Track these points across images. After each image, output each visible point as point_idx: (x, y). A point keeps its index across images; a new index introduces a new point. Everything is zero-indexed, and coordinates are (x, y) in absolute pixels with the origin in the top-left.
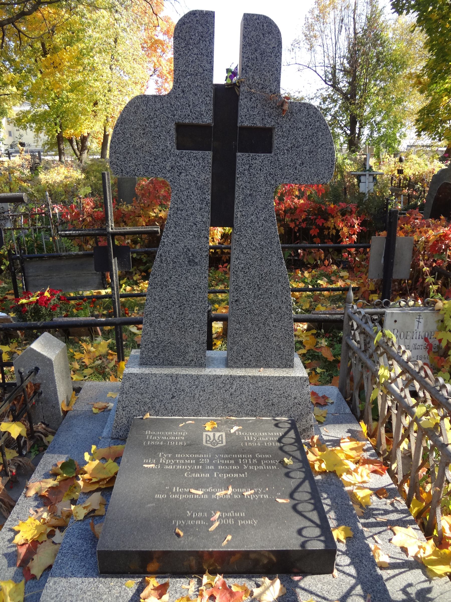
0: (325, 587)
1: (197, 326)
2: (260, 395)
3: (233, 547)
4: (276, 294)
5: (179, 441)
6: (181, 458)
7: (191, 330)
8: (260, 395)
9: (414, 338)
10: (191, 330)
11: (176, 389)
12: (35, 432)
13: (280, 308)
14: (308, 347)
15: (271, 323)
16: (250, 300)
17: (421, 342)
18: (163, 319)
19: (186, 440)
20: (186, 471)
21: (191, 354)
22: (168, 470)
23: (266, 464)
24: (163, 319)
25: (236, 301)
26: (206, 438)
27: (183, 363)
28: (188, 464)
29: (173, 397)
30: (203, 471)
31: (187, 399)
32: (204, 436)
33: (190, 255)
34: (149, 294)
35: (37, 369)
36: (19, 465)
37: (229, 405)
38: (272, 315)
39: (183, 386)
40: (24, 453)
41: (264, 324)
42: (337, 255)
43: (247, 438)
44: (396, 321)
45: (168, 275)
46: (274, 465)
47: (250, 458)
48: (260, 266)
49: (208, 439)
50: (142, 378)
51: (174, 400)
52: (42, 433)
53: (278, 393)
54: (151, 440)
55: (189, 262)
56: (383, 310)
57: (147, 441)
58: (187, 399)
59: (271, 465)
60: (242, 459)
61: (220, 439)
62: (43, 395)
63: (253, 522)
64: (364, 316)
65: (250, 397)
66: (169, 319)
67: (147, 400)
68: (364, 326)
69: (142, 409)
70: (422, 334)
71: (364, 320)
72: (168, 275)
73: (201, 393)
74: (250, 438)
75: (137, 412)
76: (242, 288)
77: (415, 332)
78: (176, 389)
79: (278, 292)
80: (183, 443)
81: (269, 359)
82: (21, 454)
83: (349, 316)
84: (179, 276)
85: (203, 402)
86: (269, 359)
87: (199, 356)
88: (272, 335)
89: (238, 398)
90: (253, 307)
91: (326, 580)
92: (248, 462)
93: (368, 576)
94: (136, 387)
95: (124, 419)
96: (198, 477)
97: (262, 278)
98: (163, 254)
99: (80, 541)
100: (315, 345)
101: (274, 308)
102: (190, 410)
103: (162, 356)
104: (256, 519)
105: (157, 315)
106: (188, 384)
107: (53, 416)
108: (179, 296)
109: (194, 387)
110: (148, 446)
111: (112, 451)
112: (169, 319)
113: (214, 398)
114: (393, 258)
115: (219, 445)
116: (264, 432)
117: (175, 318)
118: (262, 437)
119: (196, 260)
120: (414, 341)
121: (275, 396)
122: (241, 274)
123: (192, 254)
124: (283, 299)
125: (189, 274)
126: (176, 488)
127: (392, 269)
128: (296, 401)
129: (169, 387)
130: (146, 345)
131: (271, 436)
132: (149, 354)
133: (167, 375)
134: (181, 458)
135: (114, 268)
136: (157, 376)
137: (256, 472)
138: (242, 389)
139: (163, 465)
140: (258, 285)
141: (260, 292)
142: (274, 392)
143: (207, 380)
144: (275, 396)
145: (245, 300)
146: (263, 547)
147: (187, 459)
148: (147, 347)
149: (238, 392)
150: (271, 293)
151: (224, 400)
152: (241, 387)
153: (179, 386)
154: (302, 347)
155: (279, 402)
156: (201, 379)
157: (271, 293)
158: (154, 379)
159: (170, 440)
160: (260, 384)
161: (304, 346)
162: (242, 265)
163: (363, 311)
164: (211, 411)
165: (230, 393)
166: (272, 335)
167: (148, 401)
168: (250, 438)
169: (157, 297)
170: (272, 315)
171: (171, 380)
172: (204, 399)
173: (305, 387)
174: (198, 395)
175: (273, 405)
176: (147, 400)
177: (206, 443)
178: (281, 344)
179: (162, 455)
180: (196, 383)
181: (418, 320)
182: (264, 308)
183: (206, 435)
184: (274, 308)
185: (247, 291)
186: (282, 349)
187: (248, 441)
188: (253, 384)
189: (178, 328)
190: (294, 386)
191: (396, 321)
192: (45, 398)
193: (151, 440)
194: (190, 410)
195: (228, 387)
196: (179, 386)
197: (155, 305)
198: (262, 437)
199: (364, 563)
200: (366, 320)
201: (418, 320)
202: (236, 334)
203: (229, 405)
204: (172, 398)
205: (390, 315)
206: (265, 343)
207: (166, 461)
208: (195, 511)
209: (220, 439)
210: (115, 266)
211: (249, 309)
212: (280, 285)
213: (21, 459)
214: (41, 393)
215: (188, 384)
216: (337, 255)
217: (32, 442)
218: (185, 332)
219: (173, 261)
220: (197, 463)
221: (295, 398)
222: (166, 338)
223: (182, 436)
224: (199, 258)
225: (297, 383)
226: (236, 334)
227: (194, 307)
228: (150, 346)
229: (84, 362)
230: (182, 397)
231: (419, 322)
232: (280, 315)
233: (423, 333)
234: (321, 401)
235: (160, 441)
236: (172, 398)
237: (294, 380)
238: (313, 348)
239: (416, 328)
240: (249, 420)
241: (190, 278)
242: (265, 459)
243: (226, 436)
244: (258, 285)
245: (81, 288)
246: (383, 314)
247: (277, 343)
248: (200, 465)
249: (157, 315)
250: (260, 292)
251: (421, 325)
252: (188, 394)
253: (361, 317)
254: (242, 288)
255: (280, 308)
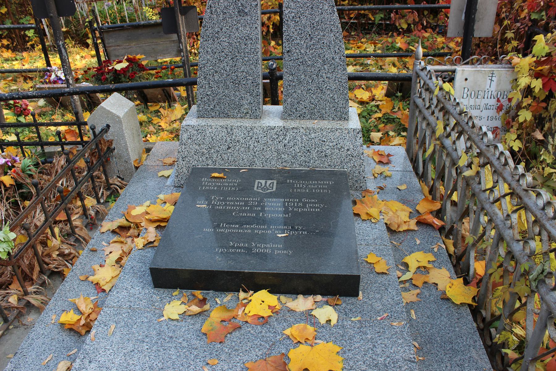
0: (348, 307)
1: (251, 78)
2: (313, 147)
3: (266, 270)
4: (328, 44)
5: (231, 187)
6: (231, 201)
7: (244, 82)
8: (313, 147)
9: (486, 97)
10: (244, 82)
11: (231, 140)
12: (112, 184)
13: (333, 58)
14: (384, 111)
15: (324, 75)
16: (302, 51)
17: (493, 102)
18: (216, 72)
19: (239, 185)
20: (234, 210)
21: (246, 106)
22: (218, 210)
23: (311, 207)
24: (216, 72)
25: (288, 52)
26: (258, 185)
27: (239, 116)
28: (237, 205)
29: (229, 148)
30: (251, 211)
31: (242, 149)
32: (256, 183)
33: (240, 5)
34: (201, 47)
35: (108, 126)
36: (98, 211)
37: (283, 155)
38: (326, 67)
39: (238, 137)
40: (102, 201)
41: (317, 76)
42: (433, 19)
43: (297, 185)
44: (466, 79)
45: (218, 27)
46: (318, 208)
47: (296, 202)
48: (311, 14)
49: (260, 185)
50: (199, 130)
51: (229, 151)
52: (117, 186)
53: (331, 144)
54: (206, 186)
55: (239, 12)
56: (453, 67)
57: (202, 186)
58: (242, 149)
59: (315, 208)
60: (288, 202)
61: (271, 186)
62: (116, 150)
63: (288, 252)
64: (429, 71)
65: (303, 148)
66: (222, 71)
67: (204, 150)
68: (428, 82)
69: (201, 159)
70: (494, 93)
71: (429, 76)
72: (218, 27)
73: (256, 144)
74: (300, 185)
75: (196, 162)
76: (293, 38)
77: (487, 91)
78: (231, 140)
79: (330, 42)
80: (236, 189)
81: (324, 112)
82: (99, 202)
83: (417, 73)
84: (230, 27)
85: (257, 153)
86: (324, 112)
87: (254, 108)
88: (326, 87)
89: (291, 149)
90: (306, 58)
91: (350, 302)
92: (294, 204)
93: (389, 300)
94: (194, 138)
95: (184, 169)
96: (244, 216)
97: (314, 27)
98: (212, 5)
99: (140, 264)
100: (391, 108)
101: (327, 59)
102: (245, 160)
103: (218, 108)
104: (291, 250)
105: (211, 67)
106: (243, 135)
107: (126, 170)
108: (231, 47)
109: (249, 138)
110: (203, 191)
111: (173, 197)
112: (222, 71)
113: (268, 149)
114: (474, 14)
115: (269, 191)
116: (314, 181)
117: (228, 70)
118: (311, 185)
119: (246, 11)
120: (486, 101)
121: (328, 147)
122: (292, 24)
123: (242, 4)
124: (336, 49)
125: (240, 25)
126: (223, 224)
127: (473, 26)
128: (349, 152)
129: (225, 138)
130: (202, 98)
131: (320, 184)
132: (205, 107)
133: (222, 127)
134: (231, 201)
135: (182, 29)
136: (213, 127)
137: (300, 213)
138: (295, 141)
139: (214, 206)
140: (310, 35)
141: (312, 43)
142: (327, 143)
143: (261, 132)
144: (328, 147)
145: (297, 51)
146: (294, 271)
147: (237, 201)
148: (203, 100)
149: (292, 144)
150: (323, 43)
151: (278, 151)
152: (294, 138)
153: (234, 137)
154: (378, 111)
155: (332, 154)
156: (255, 130)
157: (323, 43)
158: (210, 130)
159: (224, 186)
160: (313, 135)
161: (380, 110)
162: (293, 14)
163: (429, 67)
164: (266, 161)
165: (283, 145)
166: (326, 87)
167: (206, 151)
168: (300, 185)
169: (209, 50)
170: (326, 67)
171: (226, 131)
172: (259, 150)
173: (358, 139)
174: (252, 146)
175: (326, 156)
176: (204, 150)
177: (257, 189)
178: (336, 96)
179: (215, 198)
180: (251, 134)
181: (490, 78)
182: (317, 59)
183: (259, 182)
184: (327, 59)
185: (298, 41)
186: (336, 101)
187: (297, 188)
188: (306, 135)
189: (232, 81)
190: (347, 138)
191: (466, 79)
192: (118, 154)
193: (206, 186)
194: (245, 160)
195: (281, 139)
196: (234, 137)
197: (208, 57)
198: (311, 185)
199: (389, 290)
200: (431, 75)
201: (490, 78)
202: (290, 85)
203: (283, 155)
204: (228, 149)
205: (461, 72)
206: (319, 95)
207: (217, 203)
208: (238, 242)
209: (271, 186)
210: (183, 28)
211: (301, 60)
212: (332, 35)
213: (98, 206)
214: (114, 149)
215: (243, 135)
216: (433, 19)
217: (109, 193)
218: (239, 84)
219: (222, 12)
220: (246, 205)
221: (348, 150)
222: (221, 91)
223: (235, 182)
224: (248, 8)
225: (350, 135)
226: (290, 85)
227: (246, 59)
228: (205, 99)
229: (160, 126)
230: (237, 148)
231: (491, 80)
232: (333, 66)
233: (496, 93)
234: (385, 160)
235: (214, 187)
236: (228, 149)
237: (346, 131)
238: (389, 111)
239: (488, 87)
240: (302, 170)
241: (240, 29)
242: (311, 203)
243: (277, 183)
244: (310, 35)
245: (160, 56)
246: (454, 71)
247: (331, 96)
248: (248, 206)
249: (211, 67)
250: (312, 43)
251: (494, 84)
252: (243, 145)
253: (426, 73)
254: (293, 38)
255: (333, 58)
